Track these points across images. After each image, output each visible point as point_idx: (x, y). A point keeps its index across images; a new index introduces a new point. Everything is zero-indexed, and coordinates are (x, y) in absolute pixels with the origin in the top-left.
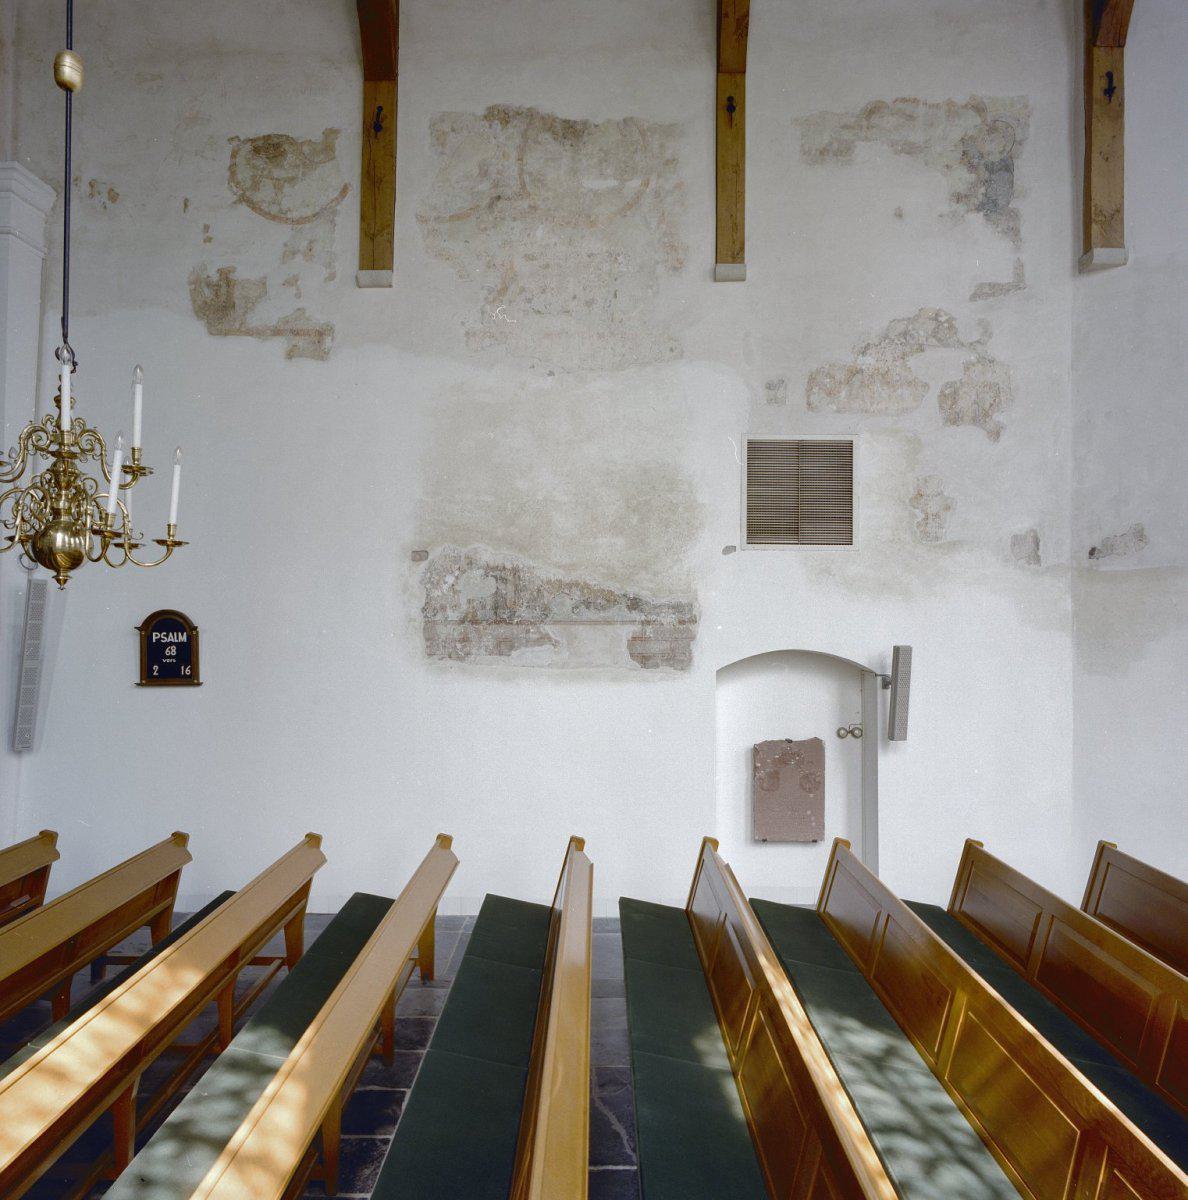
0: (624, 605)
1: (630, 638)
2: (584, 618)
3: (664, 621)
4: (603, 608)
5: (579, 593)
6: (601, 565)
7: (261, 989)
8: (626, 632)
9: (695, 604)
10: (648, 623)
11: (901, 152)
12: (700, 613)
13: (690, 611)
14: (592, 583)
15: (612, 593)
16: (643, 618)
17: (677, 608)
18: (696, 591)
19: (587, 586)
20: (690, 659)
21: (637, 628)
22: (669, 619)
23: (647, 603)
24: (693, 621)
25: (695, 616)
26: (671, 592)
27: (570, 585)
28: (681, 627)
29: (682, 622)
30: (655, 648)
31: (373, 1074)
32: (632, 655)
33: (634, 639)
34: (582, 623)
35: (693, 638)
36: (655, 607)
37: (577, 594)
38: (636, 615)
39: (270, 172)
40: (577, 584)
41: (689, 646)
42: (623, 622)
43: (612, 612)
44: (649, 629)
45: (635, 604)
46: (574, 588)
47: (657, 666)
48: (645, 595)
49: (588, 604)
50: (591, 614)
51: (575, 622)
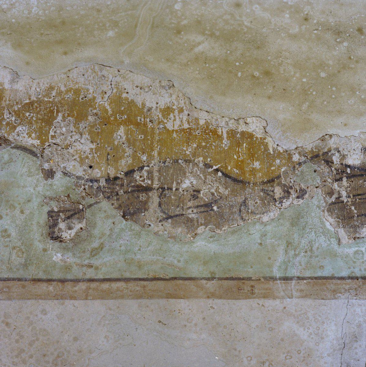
0: (317, 200)
2: (108, 263)
4: (211, 212)
5: (85, 146)
6: (199, 25)
7: (197, 207)
11: (39, 299)
14: (154, 100)
15: (254, 145)
19: (128, 113)
27: (42, 113)
34: (101, 286)
37: (76, 151)
40: (78, 107)
42: (322, 285)
43: (258, 236)
46: (61, 127)
49: (130, 196)
50: (147, 244)
51: (62, 285)
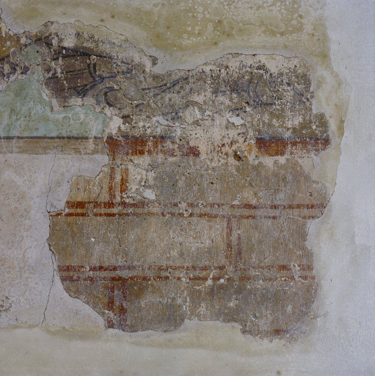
0: (38, 75)
1: (61, 205)
3: (199, 138)
8: (46, 181)
9: (319, 72)
10: (138, 144)
12: (341, 108)
13: (303, 98)
16: (116, 125)
17: (249, 88)
18: (320, 26)
20: (310, 292)
21: (93, 166)
22: (215, 130)
23: (131, 70)
24: (316, 138)
25: (322, 121)
26: (224, 29)
28: (269, 161)
29: (268, 144)
30: (160, 243)
31: (298, 169)
32: (69, 275)
33: (78, 207)
35: (318, 206)
36: (164, 84)
38: (91, 117)
39: (262, 120)
41: (303, 236)
42: (35, 143)
44: (139, 171)
45: (81, 70)
47: (171, 318)
48: (120, 38)
